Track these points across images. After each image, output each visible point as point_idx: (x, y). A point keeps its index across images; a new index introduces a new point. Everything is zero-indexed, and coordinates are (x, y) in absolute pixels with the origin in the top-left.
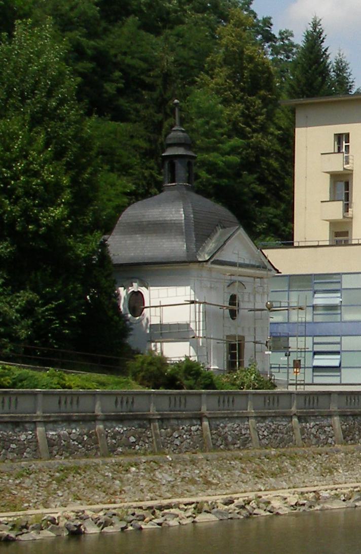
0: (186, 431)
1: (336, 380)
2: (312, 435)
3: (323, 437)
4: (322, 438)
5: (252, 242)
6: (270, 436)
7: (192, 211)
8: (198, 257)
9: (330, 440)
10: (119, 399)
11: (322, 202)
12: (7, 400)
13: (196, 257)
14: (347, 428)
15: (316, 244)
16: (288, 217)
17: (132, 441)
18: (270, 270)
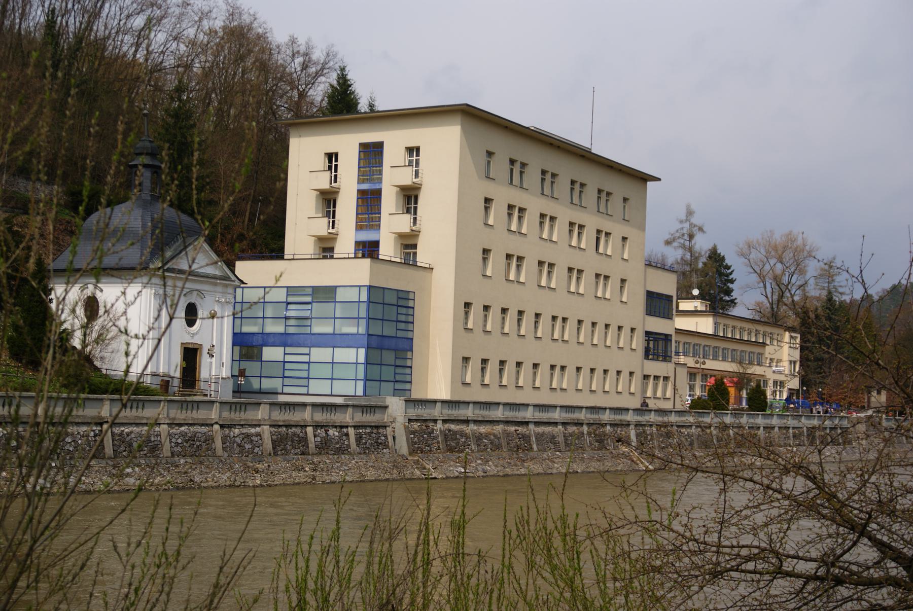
0: (83, 436)
1: (304, 390)
2: (235, 444)
3: (248, 446)
4: (247, 447)
6: (185, 444)
9: (256, 450)
10: (7, 400)
14: (277, 438)
16: (280, 235)
18: (234, 281)
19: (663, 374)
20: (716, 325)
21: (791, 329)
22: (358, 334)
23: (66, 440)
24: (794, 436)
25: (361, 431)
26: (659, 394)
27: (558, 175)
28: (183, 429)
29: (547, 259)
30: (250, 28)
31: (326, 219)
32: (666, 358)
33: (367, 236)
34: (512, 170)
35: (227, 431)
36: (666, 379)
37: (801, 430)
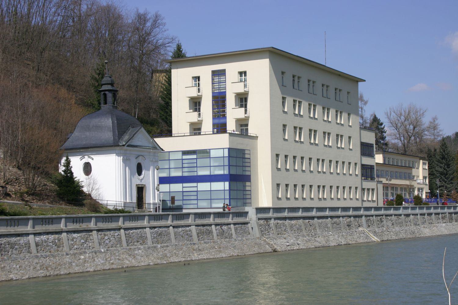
5: (148, 135)
7: (115, 119)
8: (119, 143)
11: (232, 83)
12: (219, 215)
13: (118, 143)
14: (199, 232)
15: (183, 135)
17: (82, 242)
19: (371, 187)
20: (384, 158)
21: (423, 159)
23: (105, 238)
24: (442, 218)
25: (237, 226)
26: (370, 199)
27: (301, 77)
28: (156, 229)
29: (327, 131)
31: (196, 113)
32: (372, 179)
34: (323, 89)
35: (176, 230)
36: (373, 190)
37: (446, 214)
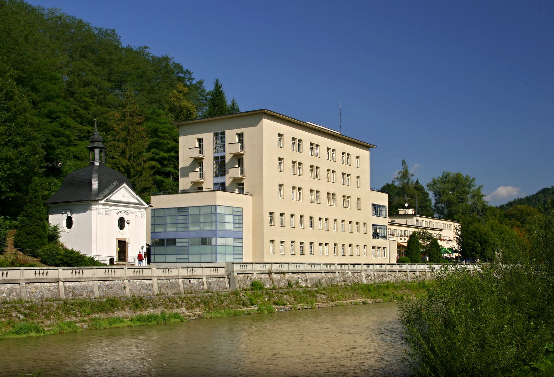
18: (145, 205)
22: (212, 230)
30: (459, 173)
33: (220, 180)
